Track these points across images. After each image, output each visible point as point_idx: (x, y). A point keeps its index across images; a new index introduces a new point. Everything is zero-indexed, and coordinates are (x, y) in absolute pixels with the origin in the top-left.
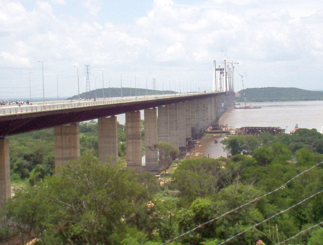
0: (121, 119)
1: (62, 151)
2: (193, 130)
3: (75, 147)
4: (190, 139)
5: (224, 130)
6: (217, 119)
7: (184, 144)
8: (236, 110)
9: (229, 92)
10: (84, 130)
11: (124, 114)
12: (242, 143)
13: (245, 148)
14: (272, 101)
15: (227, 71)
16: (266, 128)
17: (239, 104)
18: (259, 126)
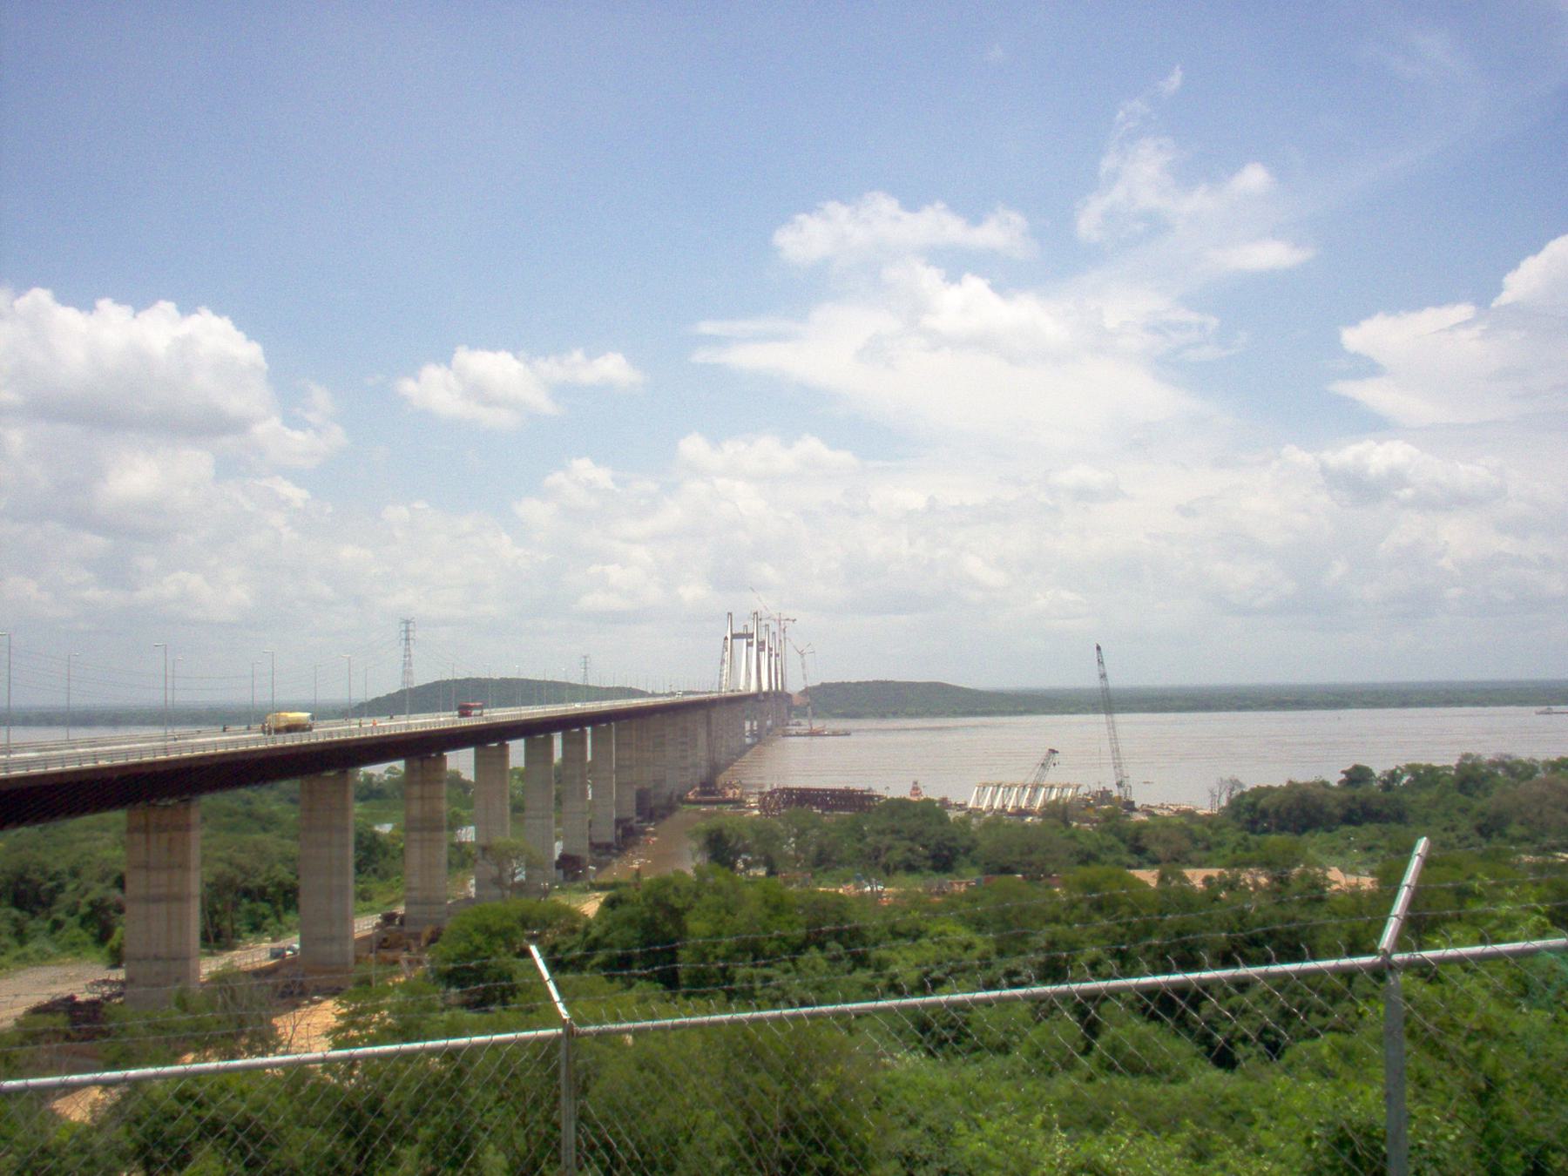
0: (461, 762)
1: (1103, 676)
2: (642, 797)
3: (184, 866)
4: (627, 820)
5: (730, 794)
6: (715, 769)
7: (608, 834)
9: (766, 694)
10: (366, 792)
11: (471, 751)
12: (740, 837)
13: (747, 850)
14: (883, 716)
16: (834, 791)
18: (823, 786)
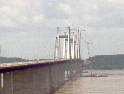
8: (82, 78)
9: (73, 60)
15: (72, 37)
17: (86, 72)
